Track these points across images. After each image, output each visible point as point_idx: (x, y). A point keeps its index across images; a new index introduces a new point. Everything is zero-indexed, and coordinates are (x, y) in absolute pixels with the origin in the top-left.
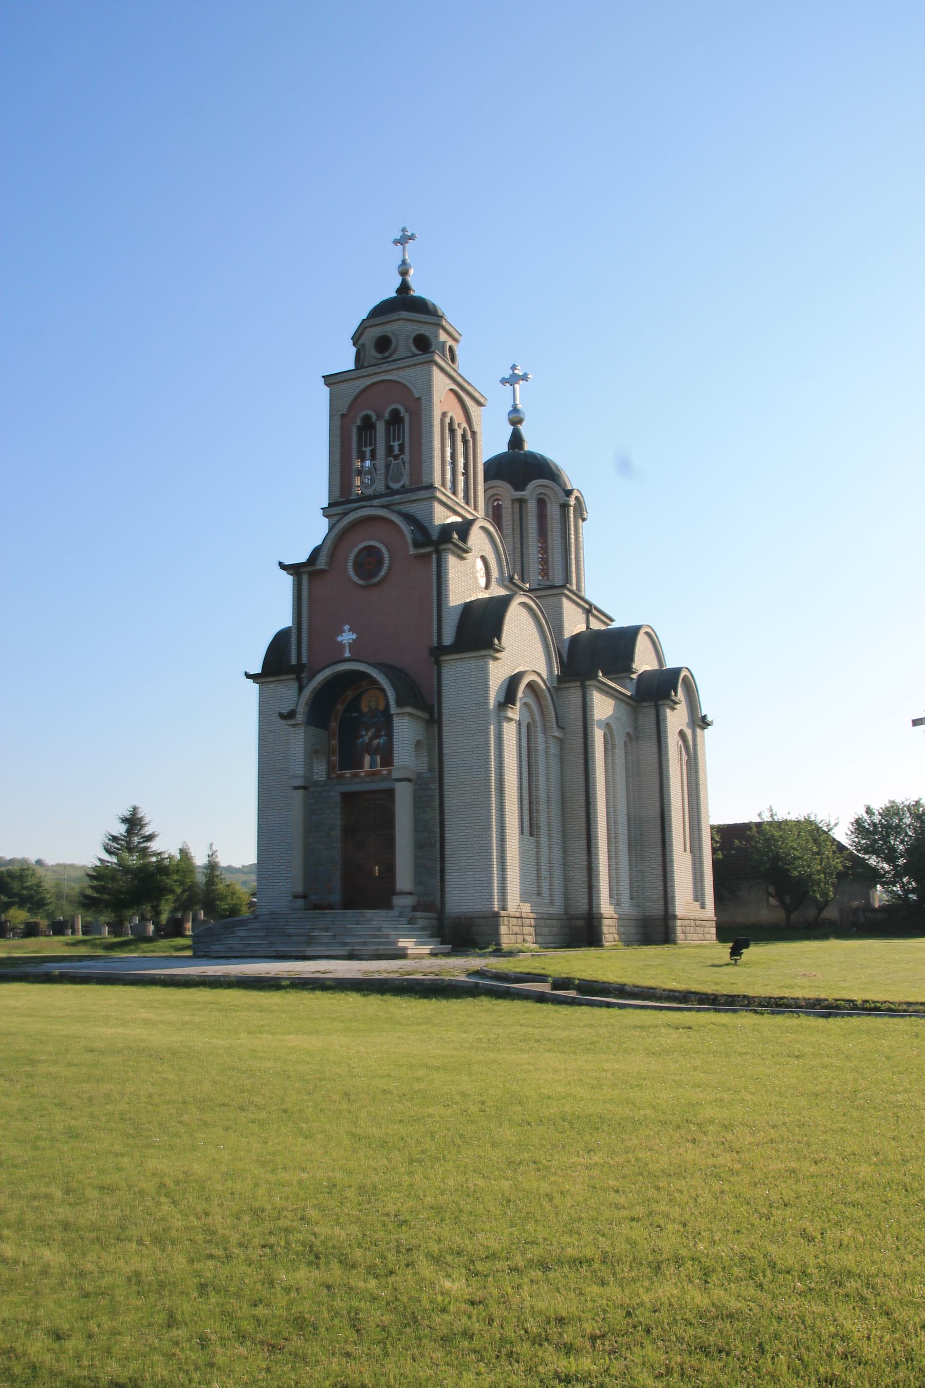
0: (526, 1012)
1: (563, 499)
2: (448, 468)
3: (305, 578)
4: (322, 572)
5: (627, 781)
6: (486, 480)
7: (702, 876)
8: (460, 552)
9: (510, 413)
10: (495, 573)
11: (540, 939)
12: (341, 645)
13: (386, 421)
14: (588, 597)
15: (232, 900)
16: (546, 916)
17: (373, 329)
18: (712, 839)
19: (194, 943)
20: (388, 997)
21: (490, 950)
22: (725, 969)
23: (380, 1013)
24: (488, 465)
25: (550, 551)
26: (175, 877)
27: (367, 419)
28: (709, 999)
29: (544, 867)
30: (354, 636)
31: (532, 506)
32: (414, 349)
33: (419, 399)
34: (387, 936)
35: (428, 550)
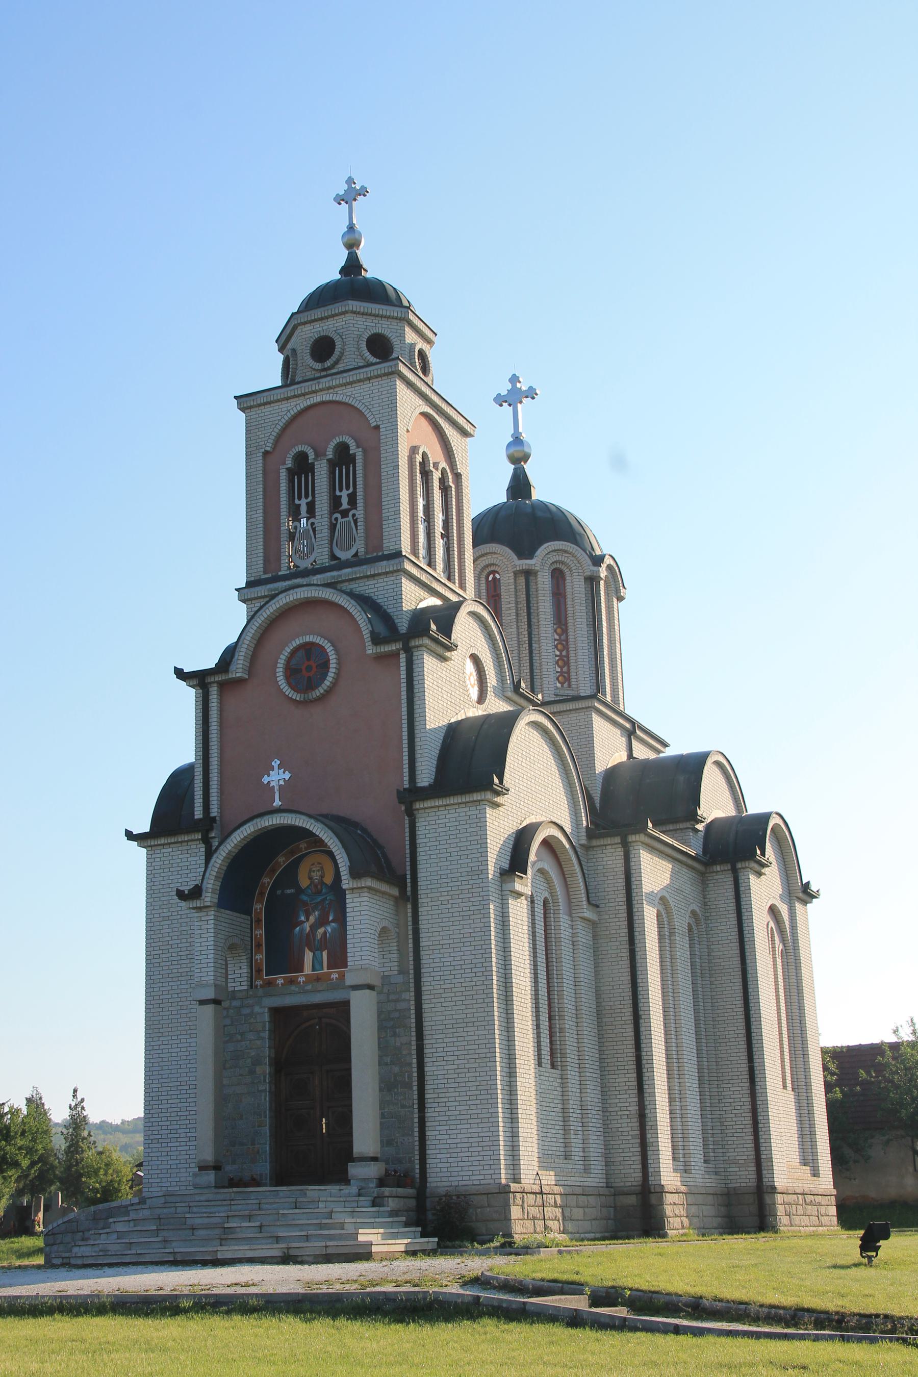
0: (552, 1343)
1: (589, 568)
2: (421, 528)
3: (214, 691)
4: (239, 681)
5: (694, 983)
6: (475, 545)
7: (812, 1126)
8: (440, 650)
9: (509, 446)
10: (492, 679)
11: (570, 1227)
12: (269, 788)
13: (329, 461)
14: (629, 711)
15: (106, 1174)
16: (578, 1190)
17: (308, 327)
18: (825, 1068)
19: (46, 1245)
20: (342, 1322)
21: (496, 1244)
22: (853, 1271)
23: (329, 1349)
24: (480, 523)
25: (571, 646)
26: (20, 1142)
27: (301, 458)
28: (830, 1320)
29: (574, 1115)
30: (287, 776)
31: (544, 582)
32: (367, 354)
33: (377, 427)
34: (342, 1226)
35: (394, 647)
